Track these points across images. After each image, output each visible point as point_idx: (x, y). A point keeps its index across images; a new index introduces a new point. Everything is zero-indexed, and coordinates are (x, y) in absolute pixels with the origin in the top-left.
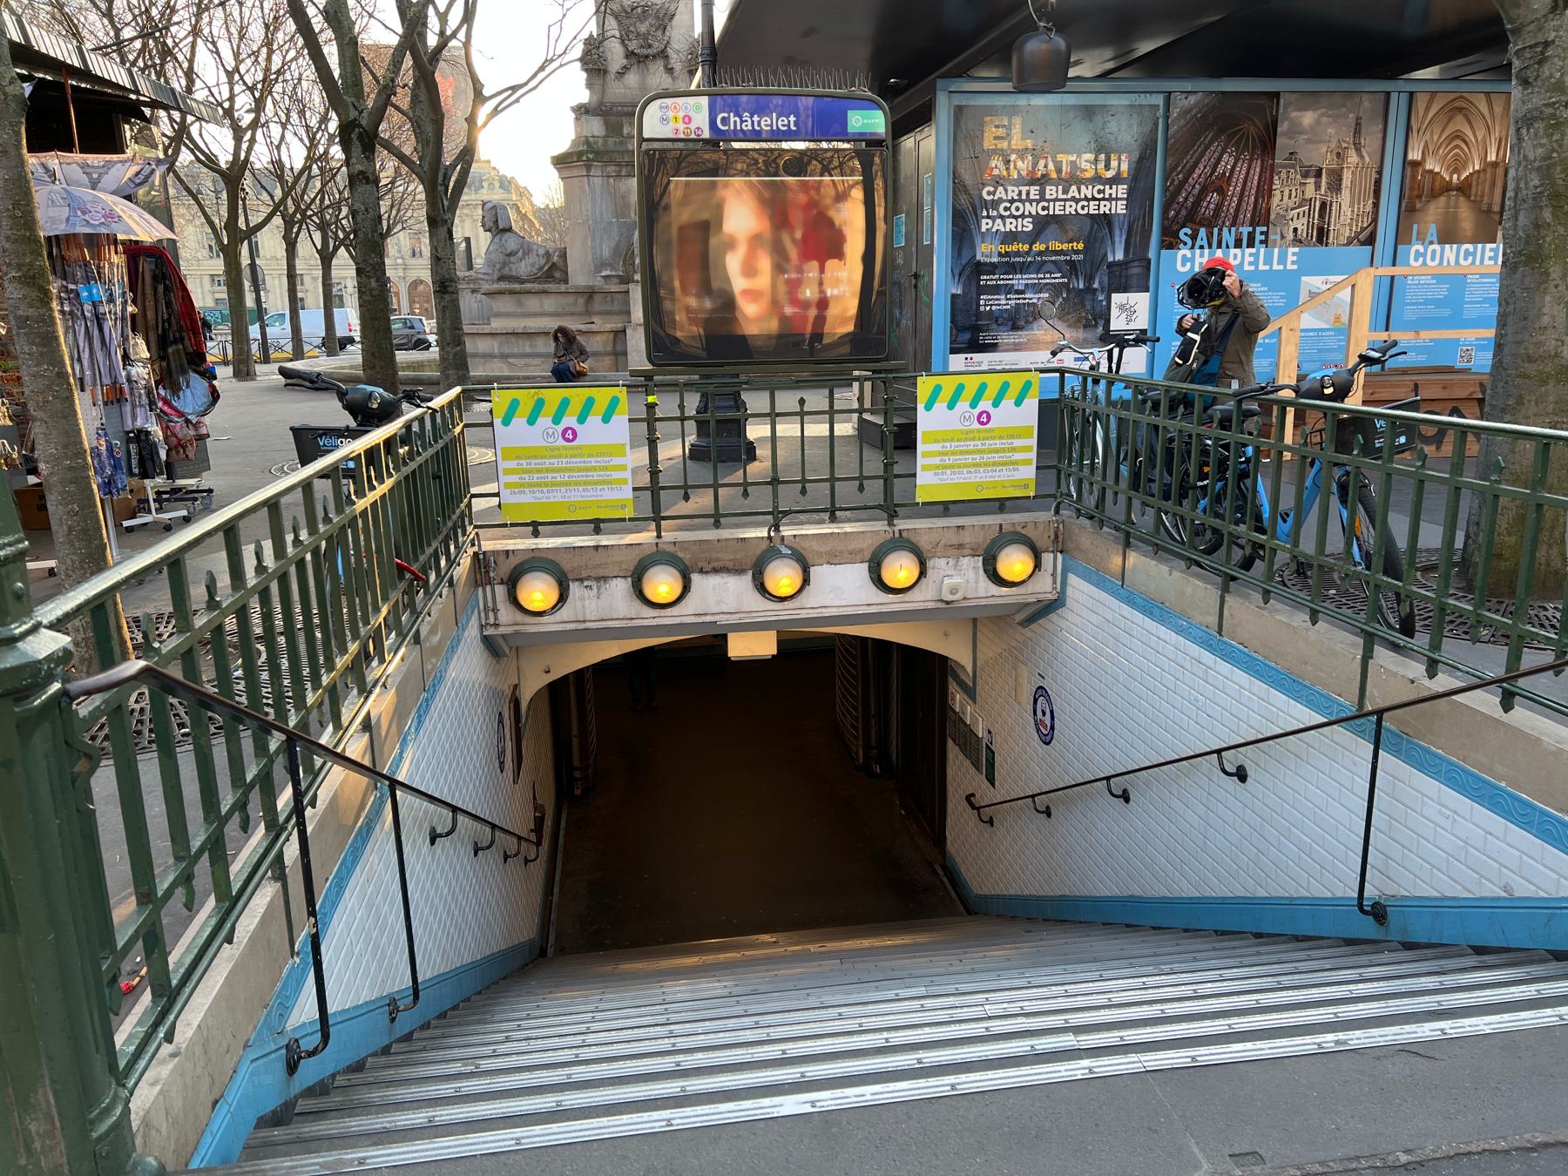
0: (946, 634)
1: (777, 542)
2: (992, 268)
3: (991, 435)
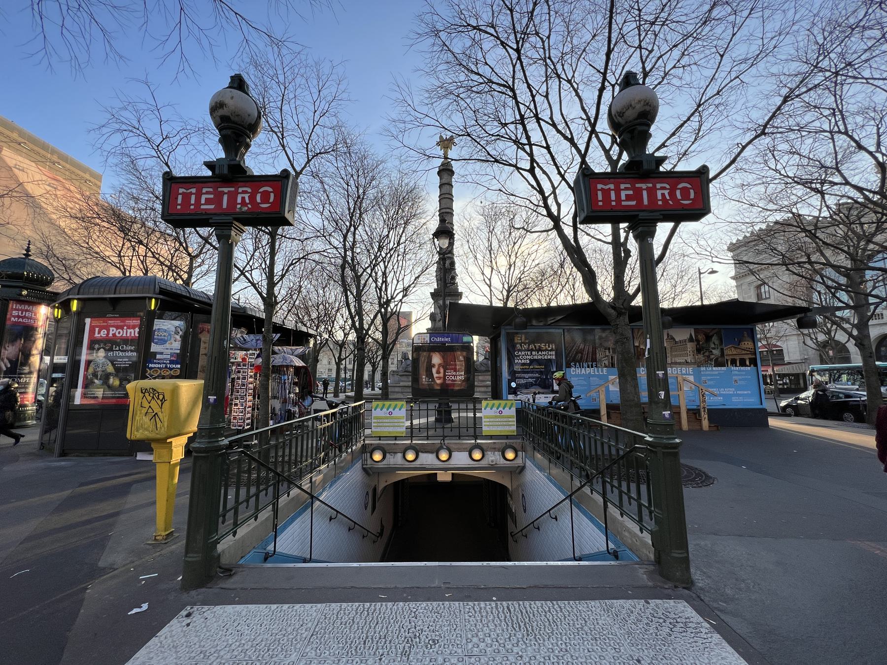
2: (519, 372)
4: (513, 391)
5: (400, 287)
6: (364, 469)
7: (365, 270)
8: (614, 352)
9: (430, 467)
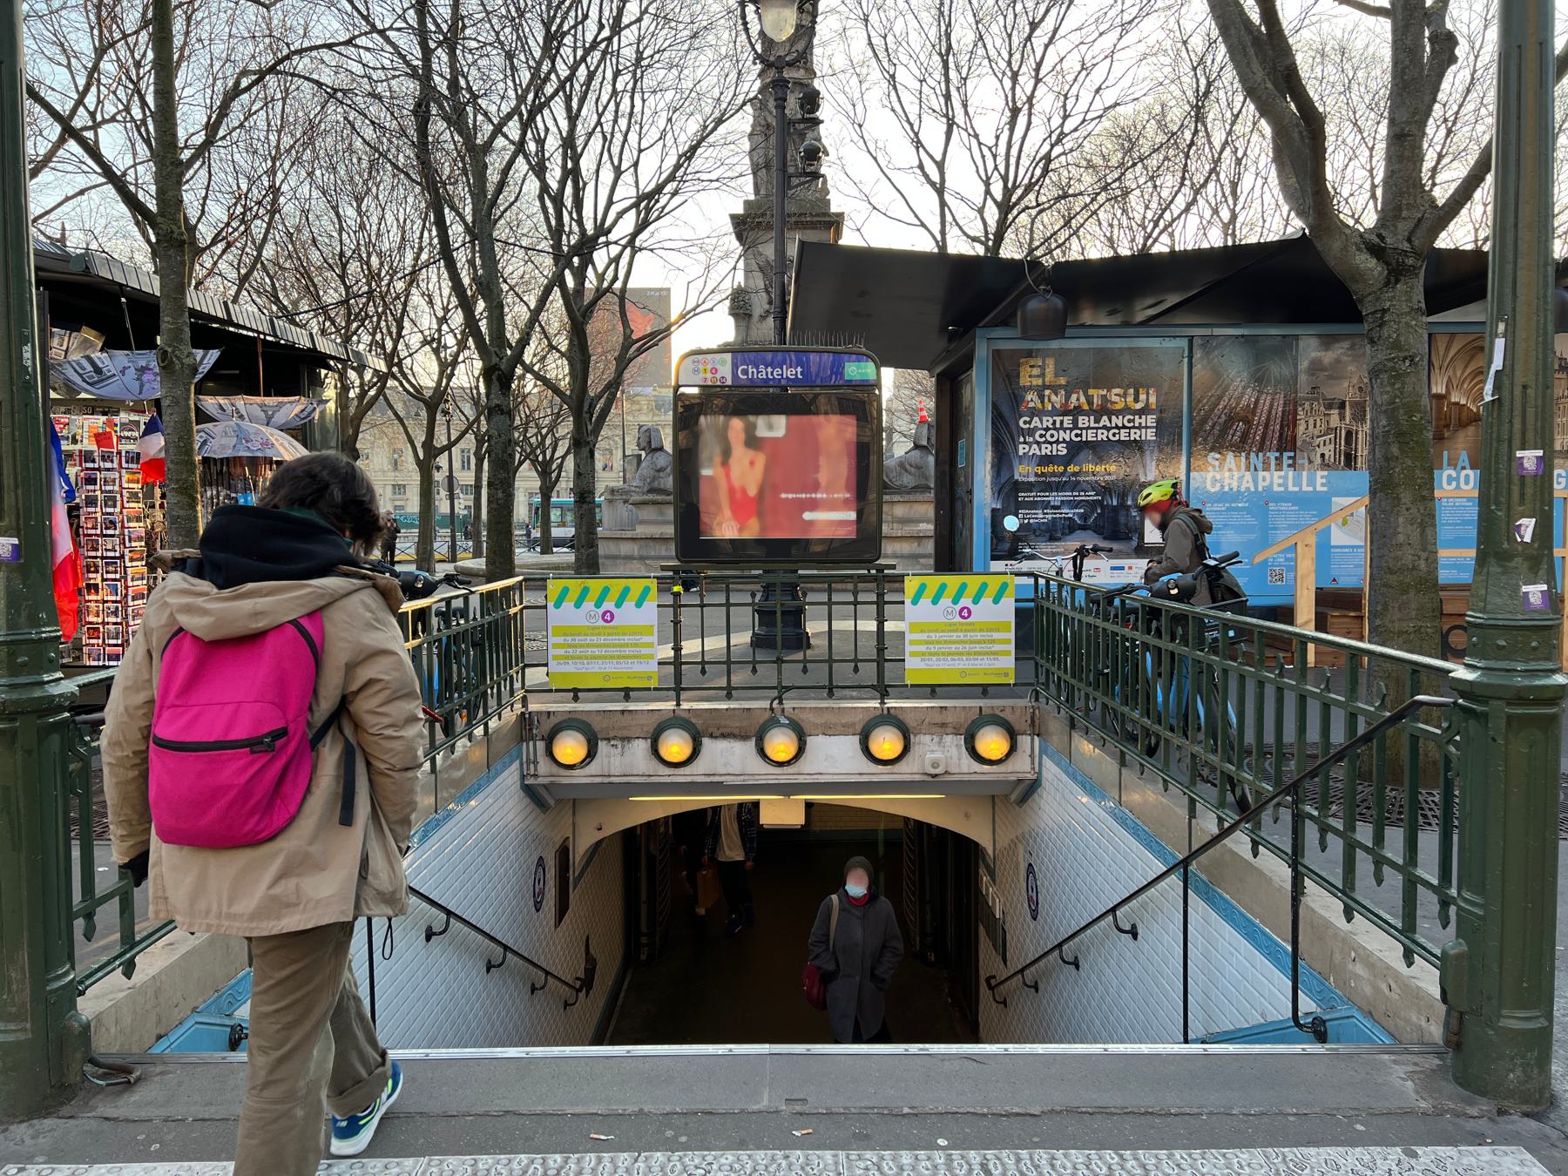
0: (967, 816)
1: (778, 712)
2: (1029, 487)
3: (973, 628)
4: (1007, 547)
5: (626, 192)
6: (530, 792)
7: (498, 130)
8: (1359, 416)
9: (738, 781)
